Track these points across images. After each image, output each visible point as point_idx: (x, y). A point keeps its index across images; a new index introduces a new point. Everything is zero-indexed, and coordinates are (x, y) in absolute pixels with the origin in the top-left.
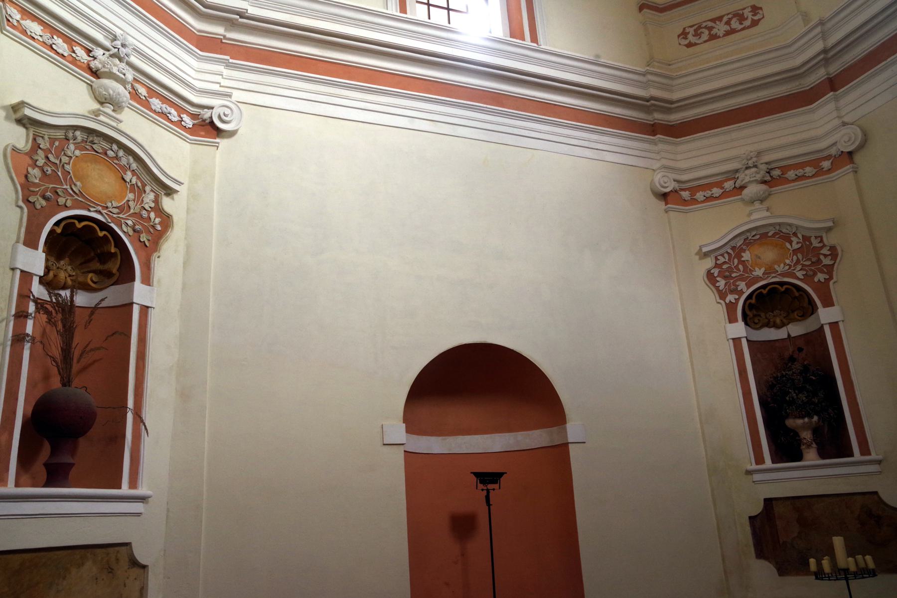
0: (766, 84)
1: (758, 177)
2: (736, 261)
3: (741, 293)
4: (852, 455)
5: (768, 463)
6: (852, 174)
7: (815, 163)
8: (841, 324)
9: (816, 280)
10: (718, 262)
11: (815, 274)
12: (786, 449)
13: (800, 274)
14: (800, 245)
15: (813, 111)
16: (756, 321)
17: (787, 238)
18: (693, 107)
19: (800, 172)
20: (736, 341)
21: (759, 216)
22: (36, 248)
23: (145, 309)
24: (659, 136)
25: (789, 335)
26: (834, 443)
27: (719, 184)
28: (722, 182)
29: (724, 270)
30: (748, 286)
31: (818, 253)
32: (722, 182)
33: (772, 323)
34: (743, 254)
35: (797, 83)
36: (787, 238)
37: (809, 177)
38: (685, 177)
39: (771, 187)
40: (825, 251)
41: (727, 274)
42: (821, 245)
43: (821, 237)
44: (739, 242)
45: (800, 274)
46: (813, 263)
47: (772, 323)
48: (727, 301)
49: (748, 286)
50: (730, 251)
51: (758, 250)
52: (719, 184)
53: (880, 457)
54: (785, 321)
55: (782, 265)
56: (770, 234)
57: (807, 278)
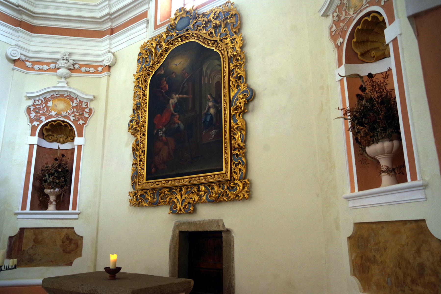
0: (84, 21)
1: (66, 65)
2: (44, 105)
3: (42, 122)
5: (28, 210)
6: (107, 77)
7: (95, 67)
8: (83, 146)
9: (78, 123)
10: (35, 104)
11: (79, 120)
13: (72, 119)
14: (77, 104)
15: (102, 42)
16: (50, 138)
17: (72, 100)
18: (51, 21)
19: (88, 69)
20: (31, 146)
22: (35, 135)
24: (18, 28)
25: (59, 148)
27: (48, 64)
28: (50, 63)
29: (36, 109)
30: (46, 120)
31: (83, 110)
32: (50, 63)
33: (58, 141)
34: (49, 102)
35: (100, 26)
38: (30, 55)
39: (72, 73)
40: (87, 110)
41: (37, 110)
42: (86, 107)
43: (87, 103)
45: (72, 119)
46: (80, 114)
47: (58, 141)
48: (33, 125)
50: (43, 99)
51: (57, 102)
52: (48, 64)
53: (79, 212)
54: (65, 140)
55: (65, 112)
56: (65, 96)
57: (75, 121)
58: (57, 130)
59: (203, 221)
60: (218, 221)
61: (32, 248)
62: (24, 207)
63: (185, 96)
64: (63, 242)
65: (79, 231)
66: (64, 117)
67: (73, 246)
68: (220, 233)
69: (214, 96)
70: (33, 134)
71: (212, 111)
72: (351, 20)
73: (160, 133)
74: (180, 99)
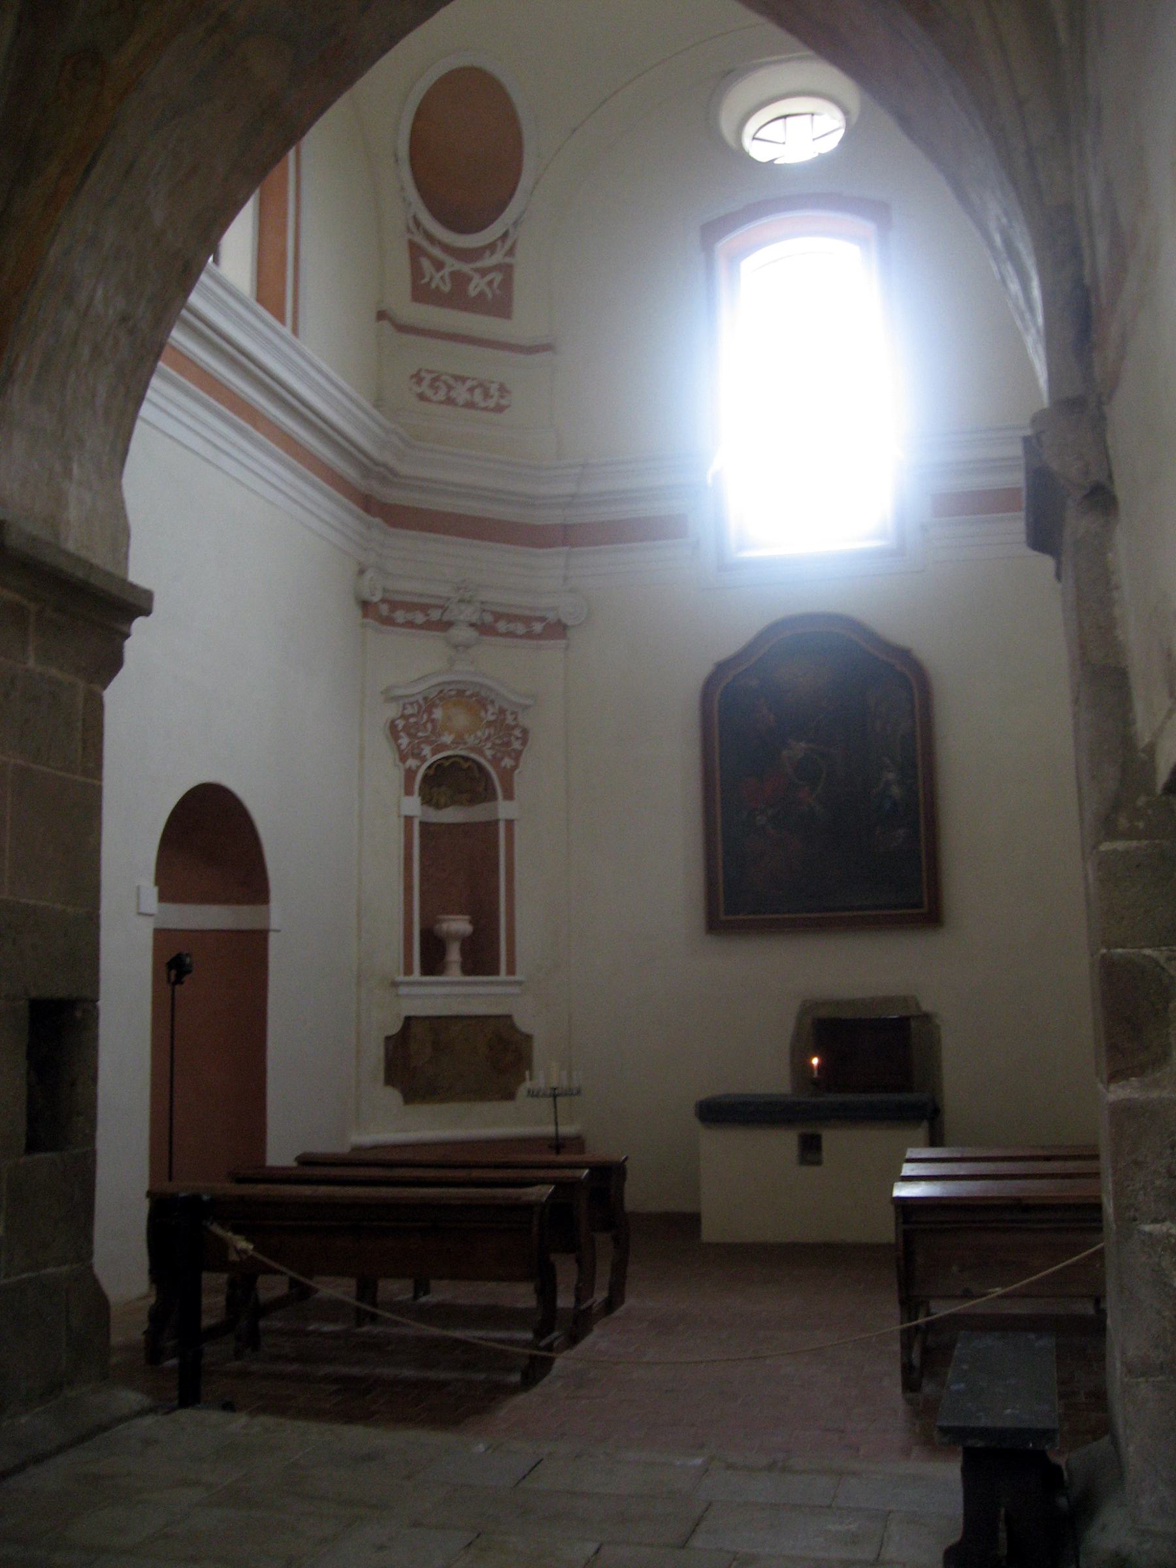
2: (425, 717)
3: (423, 760)
7: (527, 620)
13: (489, 753)
23: (510, 823)
33: (434, 801)
40: (517, 732)
45: (489, 753)
50: (421, 702)
52: (425, 608)
56: (468, 693)
57: (495, 761)
62: (408, 971)
65: (524, 1023)
66: (472, 749)
71: (896, 791)
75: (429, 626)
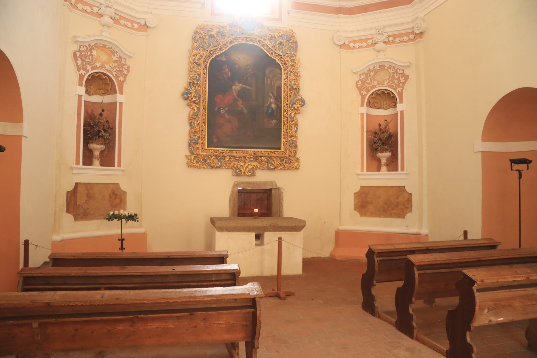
1: (382, 39)
3: (88, 71)
4: (114, 166)
7: (132, 22)
12: (374, 163)
13: (114, 74)
21: (381, 58)
23: (121, 104)
26: (393, 164)
30: (92, 69)
36: (113, 52)
37: (128, 28)
44: (93, 44)
45: (114, 74)
48: (397, 91)
49: (92, 69)
50: (88, 46)
57: (117, 77)
58: (99, 82)
59: (260, 182)
60: (271, 182)
61: (85, 202)
63: (248, 87)
64: (110, 197)
65: (123, 187)
66: (108, 71)
67: (118, 201)
68: (270, 190)
69: (275, 95)
70: (80, 84)
71: (273, 106)
72: (374, 87)
73: (222, 111)
74: (242, 89)
75: (368, 46)
